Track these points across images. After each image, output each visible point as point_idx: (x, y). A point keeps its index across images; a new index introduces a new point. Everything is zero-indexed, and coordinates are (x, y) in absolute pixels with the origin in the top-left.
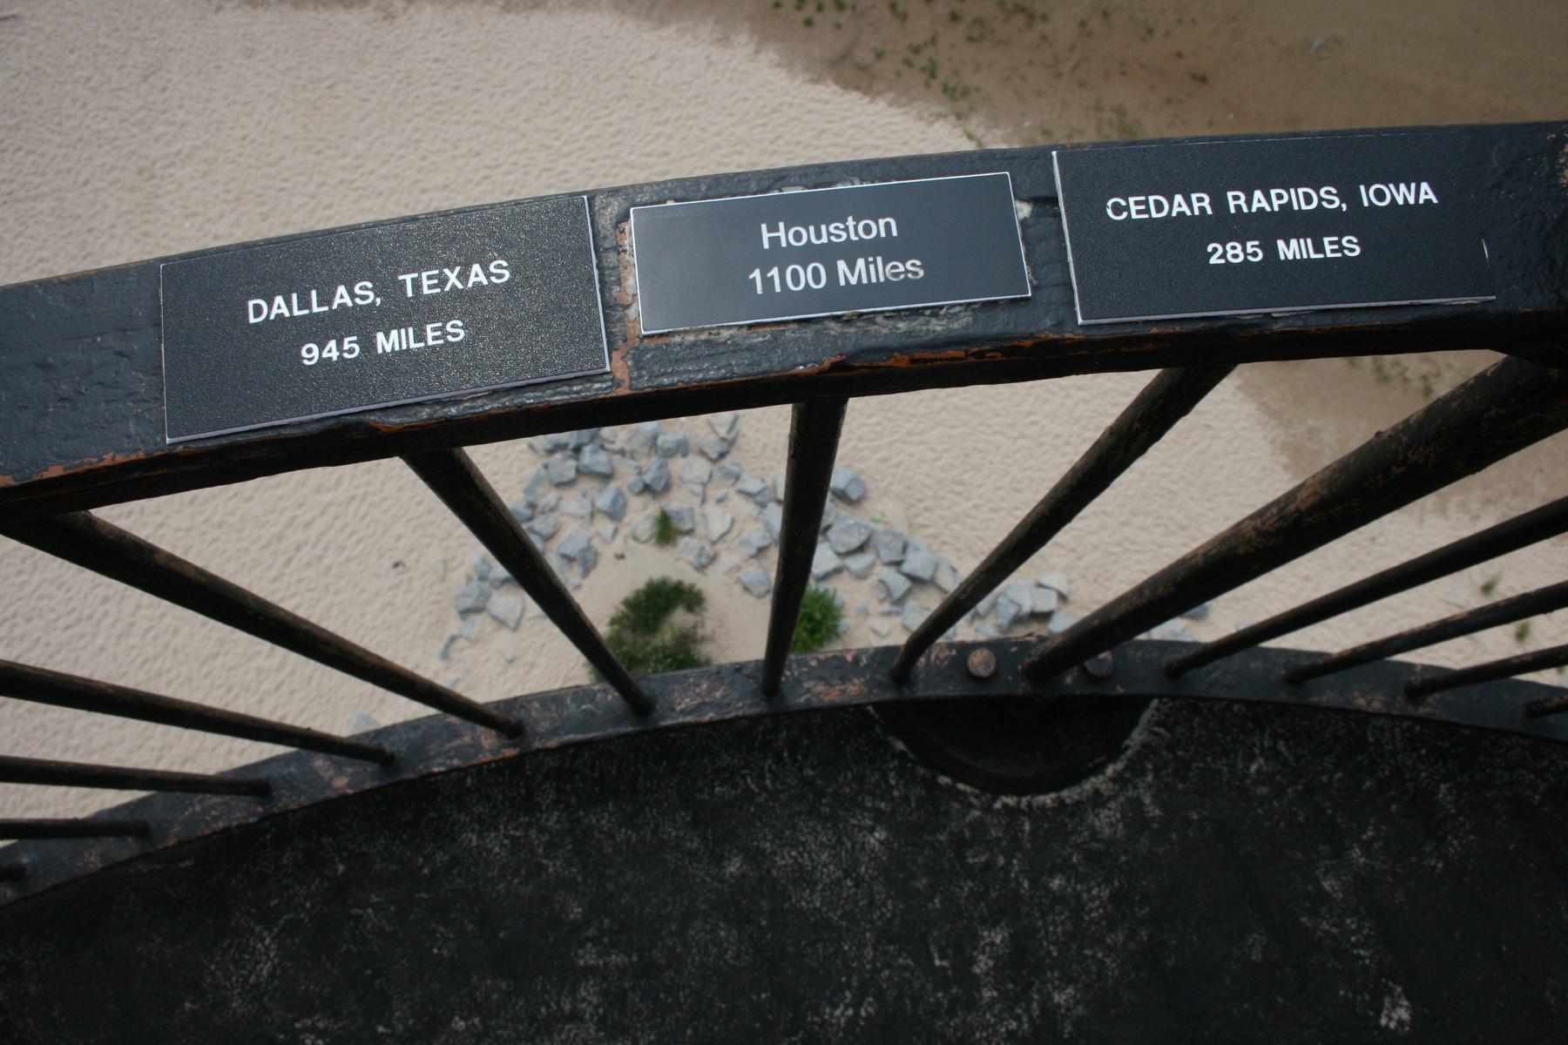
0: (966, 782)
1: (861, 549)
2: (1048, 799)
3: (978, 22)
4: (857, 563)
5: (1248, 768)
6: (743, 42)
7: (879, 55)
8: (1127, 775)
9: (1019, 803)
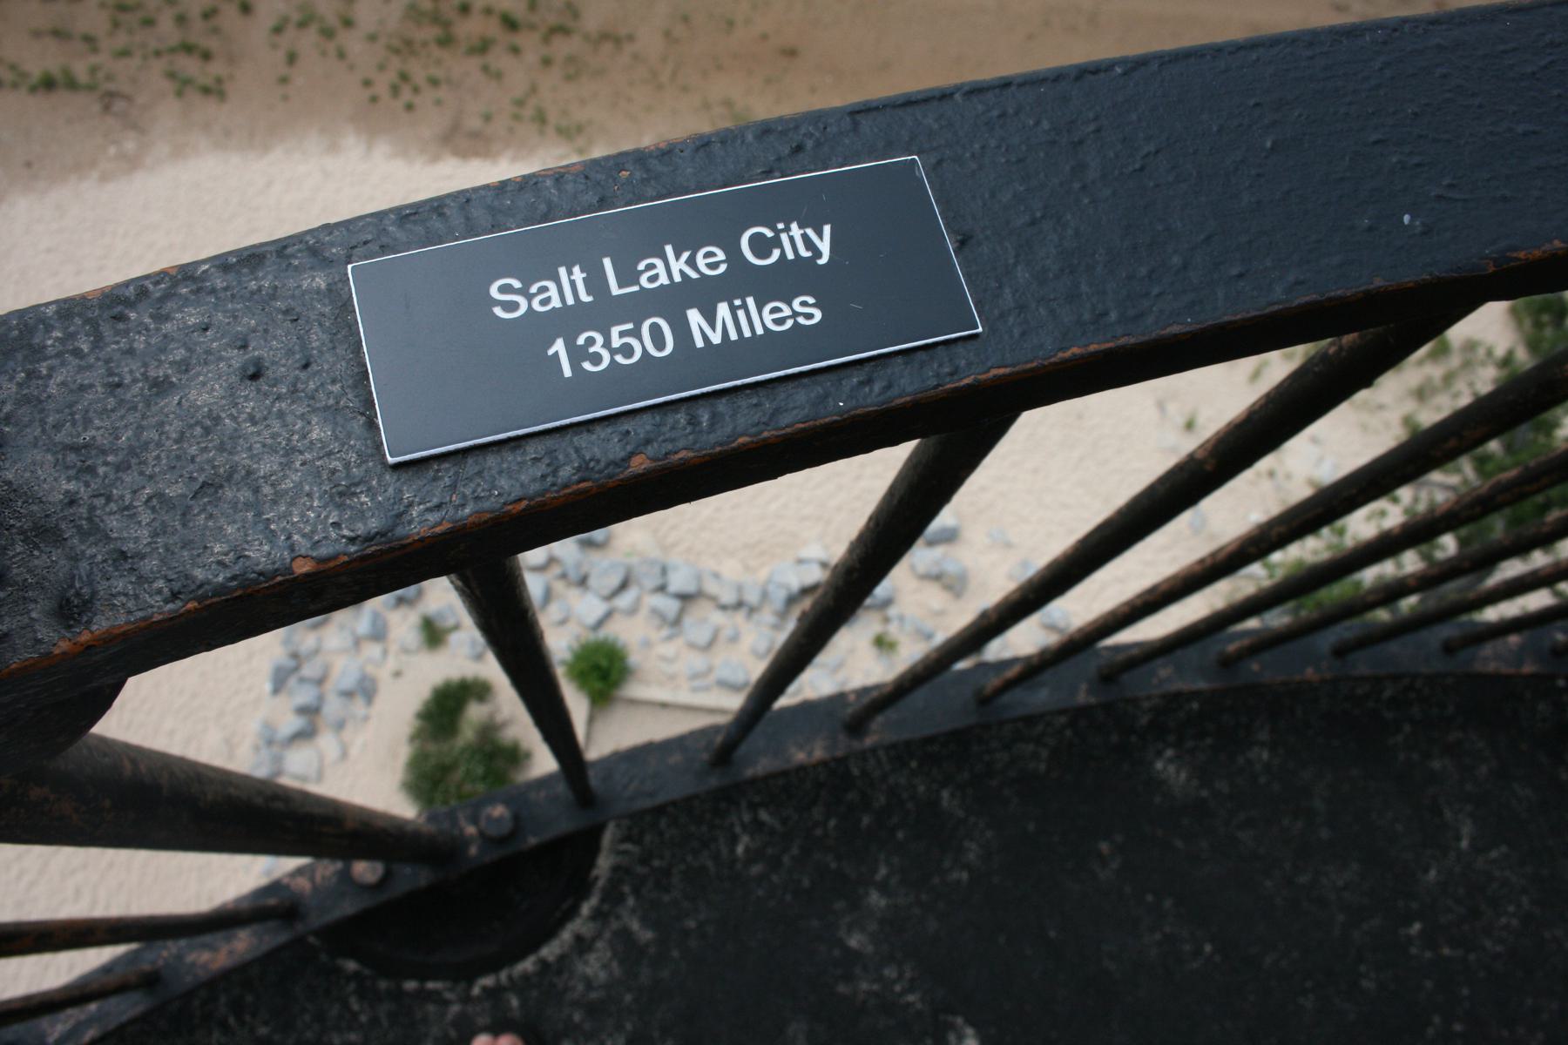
0: (435, 978)
1: (624, 586)
2: (528, 965)
3: (571, 60)
4: (624, 601)
5: (732, 851)
6: (352, 144)
7: (488, 118)
8: (606, 907)
9: (498, 980)
